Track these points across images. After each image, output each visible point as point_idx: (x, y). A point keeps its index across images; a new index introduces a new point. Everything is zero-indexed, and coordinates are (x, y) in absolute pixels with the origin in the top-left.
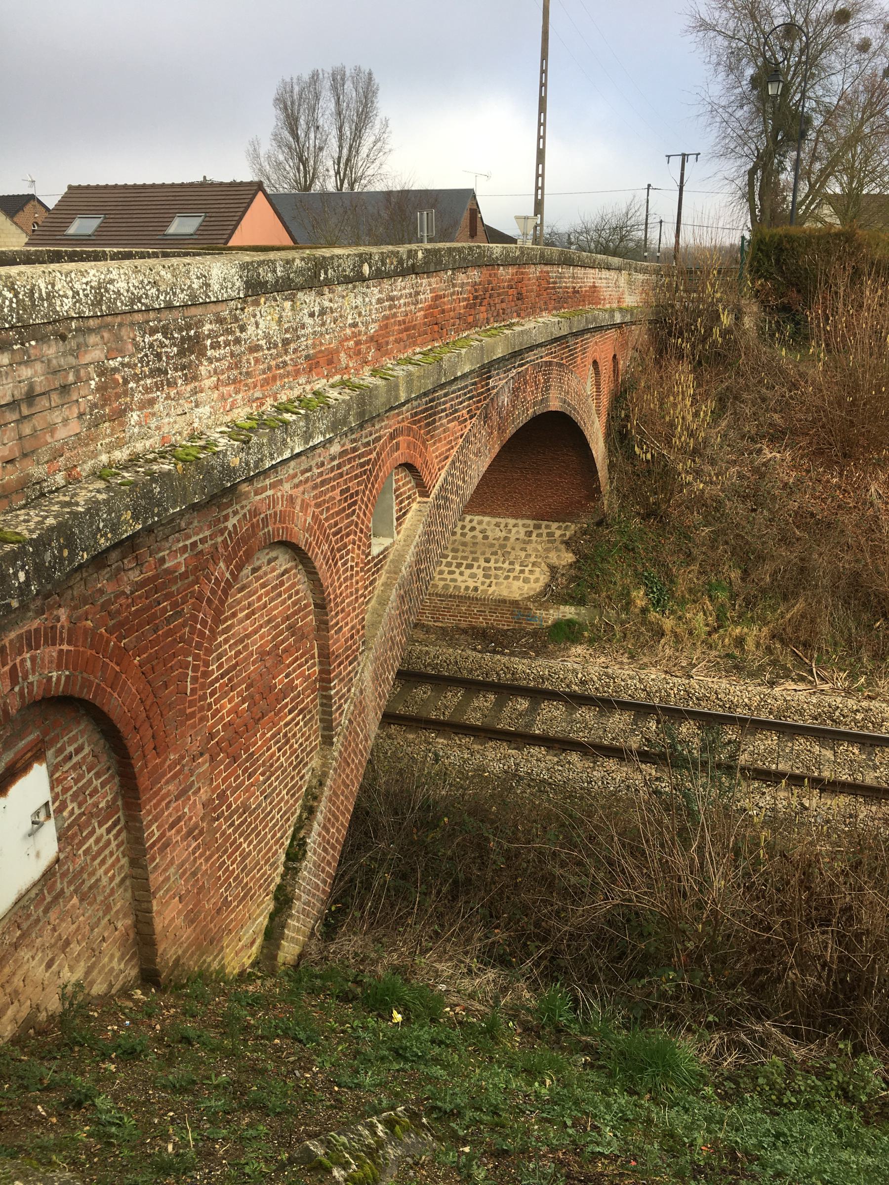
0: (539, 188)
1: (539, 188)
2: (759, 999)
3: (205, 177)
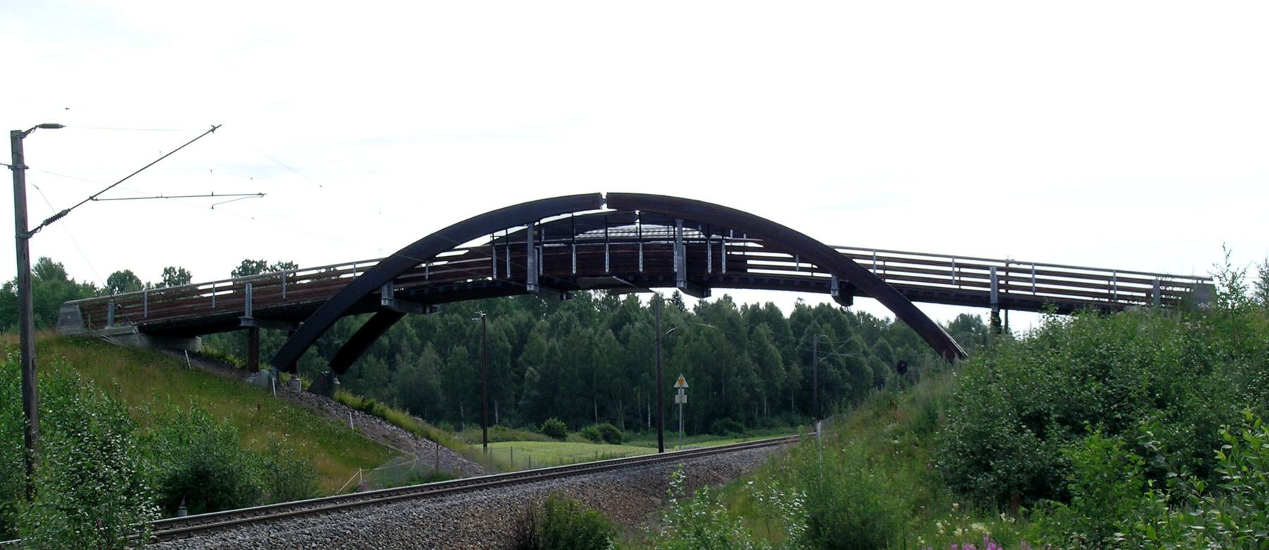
0: (512, 457)
1: (512, 457)
2: (382, 471)
3: (27, 168)
